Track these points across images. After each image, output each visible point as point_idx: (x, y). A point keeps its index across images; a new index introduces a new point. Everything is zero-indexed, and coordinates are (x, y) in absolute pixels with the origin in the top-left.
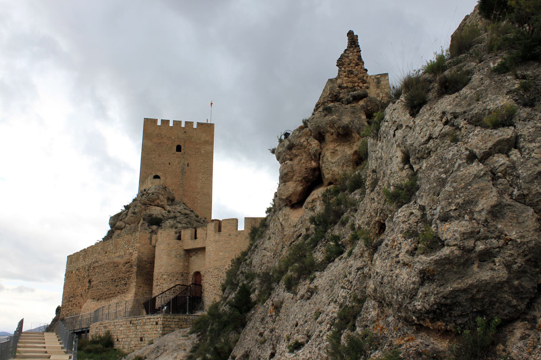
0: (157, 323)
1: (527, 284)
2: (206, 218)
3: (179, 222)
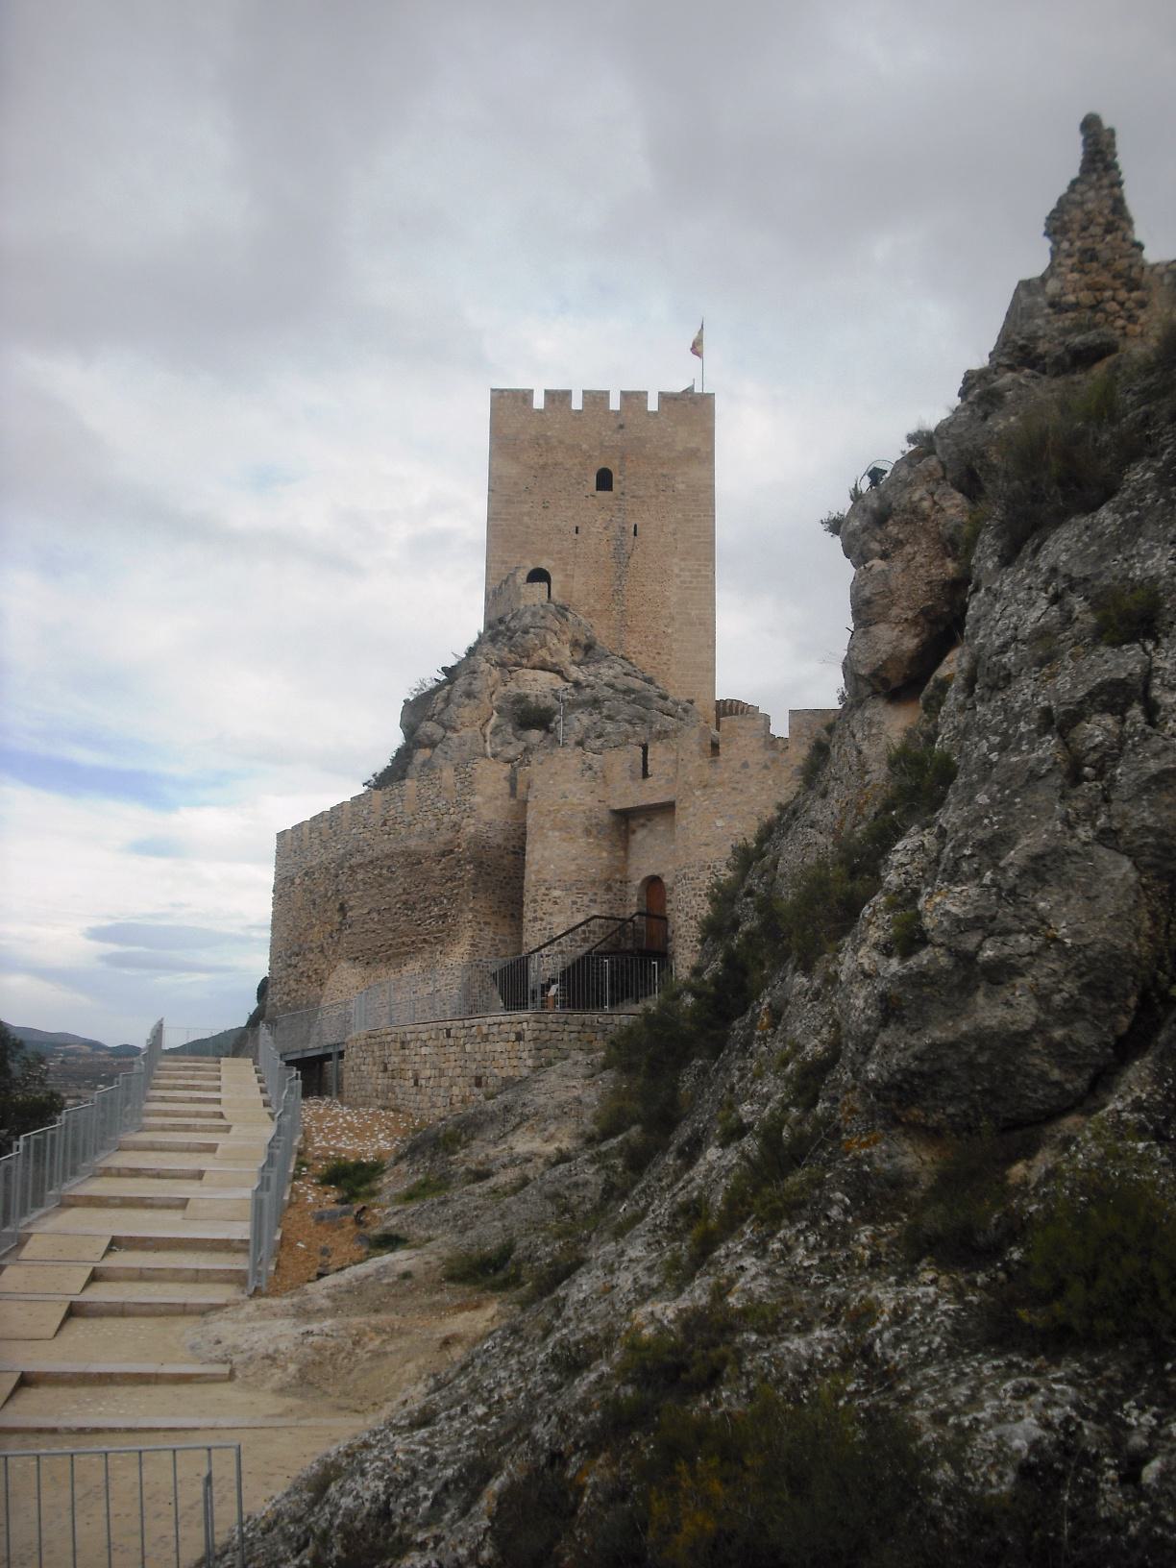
0: (519, 1037)
1: (1084, 1035)
2: (691, 702)
3: (609, 718)
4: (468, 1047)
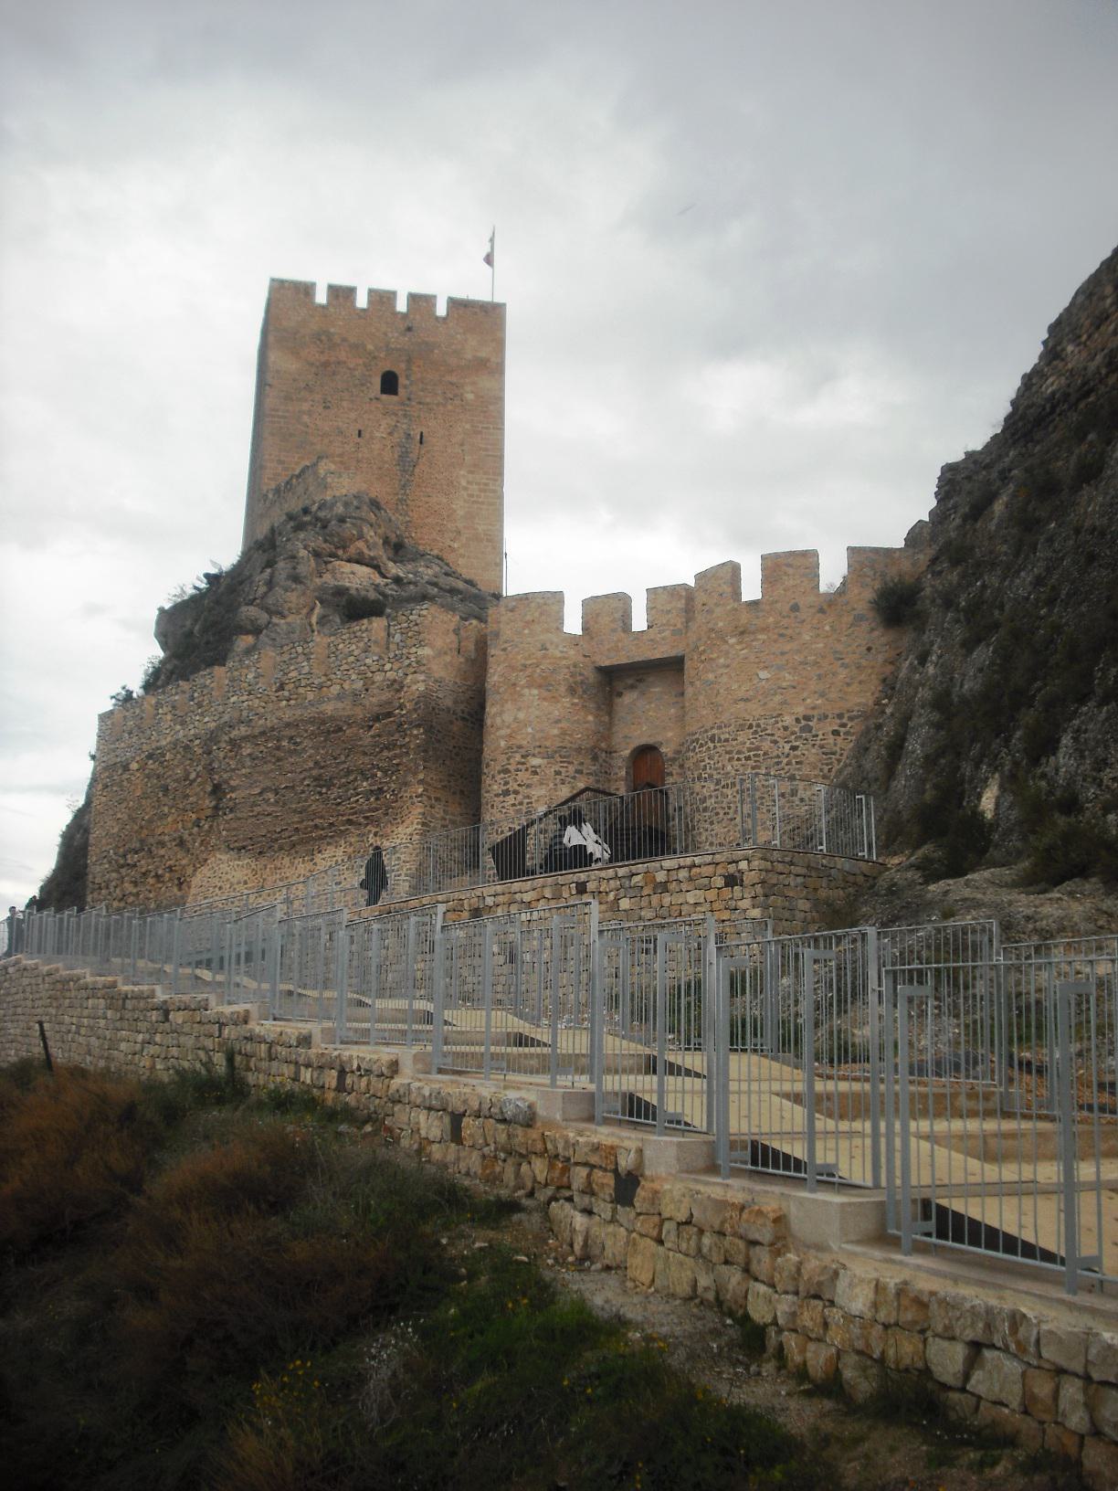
0: (731, 881)
4: (625, 904)
